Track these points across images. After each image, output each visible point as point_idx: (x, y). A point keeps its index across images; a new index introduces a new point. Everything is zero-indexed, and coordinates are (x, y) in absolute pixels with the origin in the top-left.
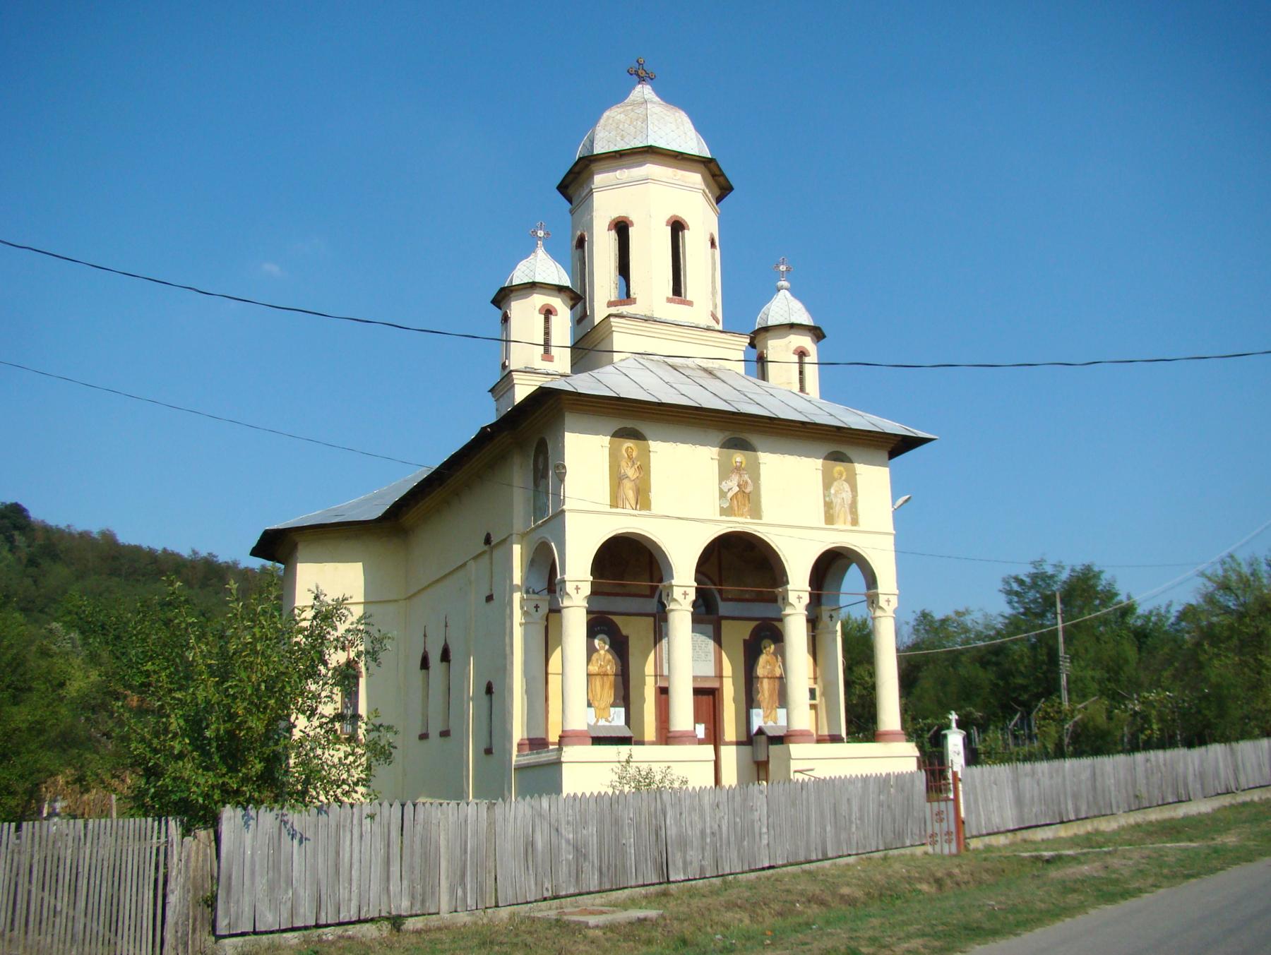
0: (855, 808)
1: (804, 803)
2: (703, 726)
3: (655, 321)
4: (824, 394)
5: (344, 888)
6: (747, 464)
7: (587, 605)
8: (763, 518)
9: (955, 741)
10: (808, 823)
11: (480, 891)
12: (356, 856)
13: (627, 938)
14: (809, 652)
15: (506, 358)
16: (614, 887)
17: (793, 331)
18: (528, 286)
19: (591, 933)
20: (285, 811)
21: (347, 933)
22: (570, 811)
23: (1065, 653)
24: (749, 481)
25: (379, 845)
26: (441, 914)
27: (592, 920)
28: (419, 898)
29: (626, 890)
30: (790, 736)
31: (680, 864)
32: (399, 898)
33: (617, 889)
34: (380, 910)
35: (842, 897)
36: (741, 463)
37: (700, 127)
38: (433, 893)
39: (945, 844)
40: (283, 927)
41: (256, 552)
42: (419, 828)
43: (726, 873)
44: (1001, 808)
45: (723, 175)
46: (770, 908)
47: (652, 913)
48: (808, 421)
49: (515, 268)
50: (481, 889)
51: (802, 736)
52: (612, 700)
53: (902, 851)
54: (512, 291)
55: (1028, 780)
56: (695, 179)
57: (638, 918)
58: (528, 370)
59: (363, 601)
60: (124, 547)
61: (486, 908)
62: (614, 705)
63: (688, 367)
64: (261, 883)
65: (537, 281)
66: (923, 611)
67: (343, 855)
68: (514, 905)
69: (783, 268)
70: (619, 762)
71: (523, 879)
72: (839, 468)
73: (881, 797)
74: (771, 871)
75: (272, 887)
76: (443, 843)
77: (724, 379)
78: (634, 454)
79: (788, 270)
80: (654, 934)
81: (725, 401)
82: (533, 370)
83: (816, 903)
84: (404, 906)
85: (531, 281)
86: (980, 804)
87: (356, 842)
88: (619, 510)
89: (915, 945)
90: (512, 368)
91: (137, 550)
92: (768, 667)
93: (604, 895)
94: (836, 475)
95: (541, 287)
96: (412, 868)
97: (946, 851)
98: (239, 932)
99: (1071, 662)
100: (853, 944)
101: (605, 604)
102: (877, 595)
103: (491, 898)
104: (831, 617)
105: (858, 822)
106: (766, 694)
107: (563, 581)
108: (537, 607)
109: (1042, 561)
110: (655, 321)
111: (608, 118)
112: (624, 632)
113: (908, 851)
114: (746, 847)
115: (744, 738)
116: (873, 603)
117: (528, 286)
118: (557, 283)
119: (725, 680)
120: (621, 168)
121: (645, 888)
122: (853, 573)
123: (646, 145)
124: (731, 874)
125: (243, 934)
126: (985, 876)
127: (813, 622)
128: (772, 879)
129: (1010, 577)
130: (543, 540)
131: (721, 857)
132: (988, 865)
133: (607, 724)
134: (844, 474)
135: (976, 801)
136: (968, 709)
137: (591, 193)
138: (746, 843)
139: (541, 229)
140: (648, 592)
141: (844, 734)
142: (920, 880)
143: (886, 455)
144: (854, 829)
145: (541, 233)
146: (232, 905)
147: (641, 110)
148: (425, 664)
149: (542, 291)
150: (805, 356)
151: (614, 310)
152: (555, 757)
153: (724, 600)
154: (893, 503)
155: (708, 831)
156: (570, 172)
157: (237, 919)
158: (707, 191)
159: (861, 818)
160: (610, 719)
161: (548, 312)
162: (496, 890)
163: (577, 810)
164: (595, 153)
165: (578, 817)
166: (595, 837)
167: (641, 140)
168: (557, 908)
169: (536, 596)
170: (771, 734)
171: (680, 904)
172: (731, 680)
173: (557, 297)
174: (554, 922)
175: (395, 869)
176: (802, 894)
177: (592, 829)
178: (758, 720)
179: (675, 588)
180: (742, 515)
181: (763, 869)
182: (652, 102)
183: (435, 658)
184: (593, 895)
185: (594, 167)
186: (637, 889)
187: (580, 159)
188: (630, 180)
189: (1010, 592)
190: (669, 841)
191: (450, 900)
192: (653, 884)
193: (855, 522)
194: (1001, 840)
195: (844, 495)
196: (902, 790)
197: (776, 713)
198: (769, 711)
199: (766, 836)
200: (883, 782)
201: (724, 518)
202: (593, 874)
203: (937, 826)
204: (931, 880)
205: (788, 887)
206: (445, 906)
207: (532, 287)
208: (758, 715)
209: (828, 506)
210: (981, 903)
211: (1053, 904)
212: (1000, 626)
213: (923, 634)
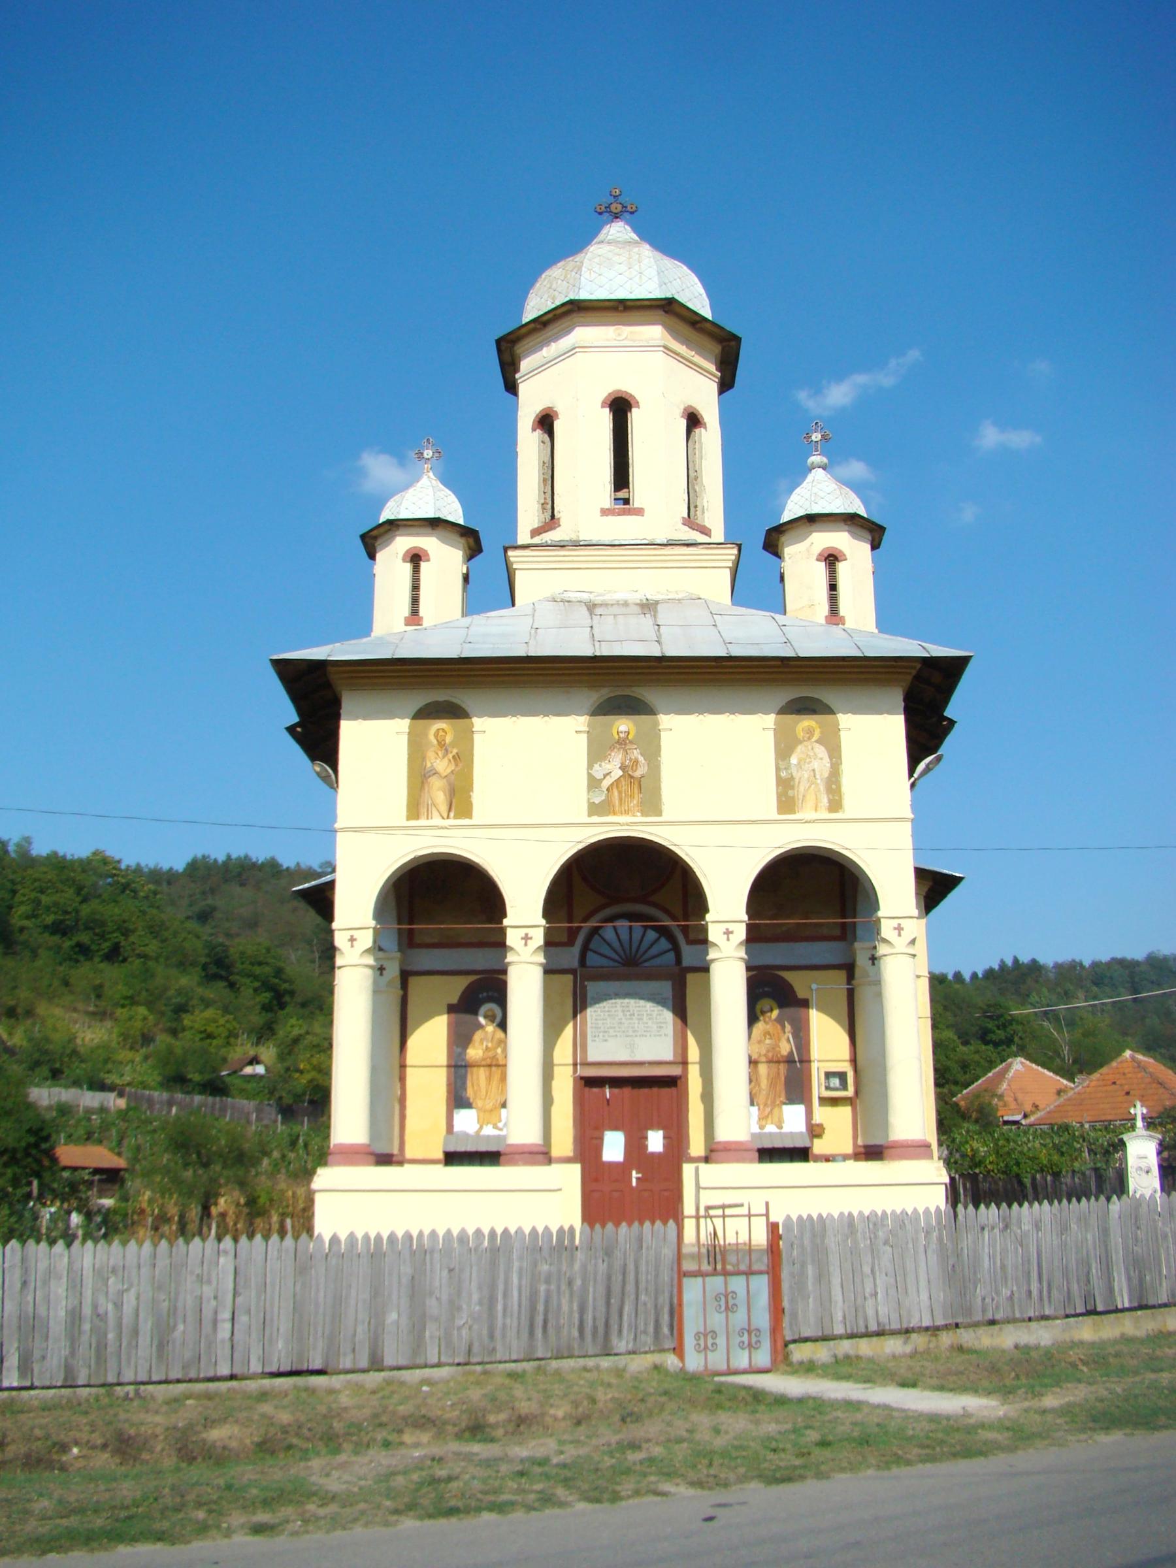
2: (661, 1133)
7: (746, 957)
8: (664, 814)
17: (817, 526)
24: (641, 759)
78: (448, 739)
79: (825, 438)
88: (422, 822)
92: (768, 1041)
95: (405, 526)
101: (775, 954)
119: (690, 1067)
120: (547, 342)
150: (838, 561)
160: (500, 1125)
161: (831, 559)
180: (627, 812)
185: (519, 348)
193: (835, 805)
195: (816, 765)
197: (781, 1112)
198: (768, 1110)
201: (595, 819)
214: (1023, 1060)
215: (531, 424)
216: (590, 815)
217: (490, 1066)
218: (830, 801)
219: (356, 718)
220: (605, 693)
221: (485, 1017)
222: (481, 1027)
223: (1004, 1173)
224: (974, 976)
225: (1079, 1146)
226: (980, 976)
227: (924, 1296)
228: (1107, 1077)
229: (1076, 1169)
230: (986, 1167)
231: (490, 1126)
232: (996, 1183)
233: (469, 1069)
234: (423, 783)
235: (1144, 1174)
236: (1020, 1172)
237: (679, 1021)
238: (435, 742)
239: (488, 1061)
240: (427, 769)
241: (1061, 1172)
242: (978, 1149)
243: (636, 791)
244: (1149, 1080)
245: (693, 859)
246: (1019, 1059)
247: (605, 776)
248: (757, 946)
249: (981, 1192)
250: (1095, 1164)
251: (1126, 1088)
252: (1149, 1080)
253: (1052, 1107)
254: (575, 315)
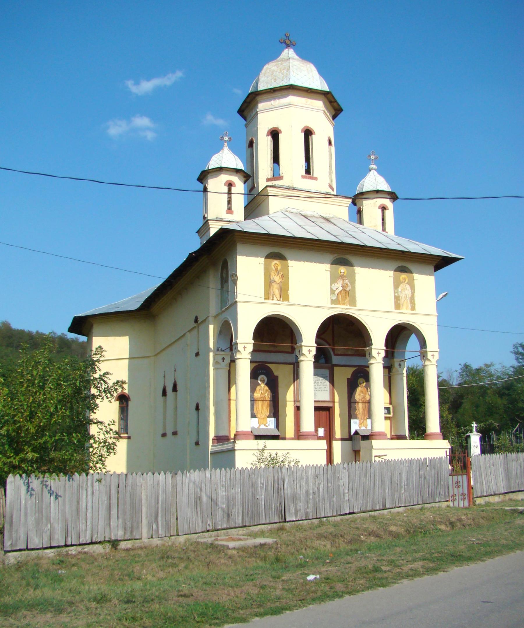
0: (404, 479)
1: (372, 475)
2: (323, 429)
3: (295, 189)
4: (397, 232)
5: (82, 524)
6: (347, 273)
7: (251, 358)
8: (357, 306)
9: (475, 439)
10: (374, 488)
11: (168, 527)
12: (90, 505)
13: (252, 555)
14: (385, 387)
15: (206, 213)
16: (251, 524)
18: (218, 169)
19: (230, 552)
20: (46, 479)
21: (84, 550)
22: (224, 479)
24: (349, 283)
25: (104, 498)
26: (143, 539)
27: (231, 544)
28: (129, 529)
29: (259, 526)
30: (373, 435)
31: (293, 511)
32: (116, 530)
33: (255, 525)
34: (105, 537)
35: (390, 532)
36: (344, 273)
37: (322, 72)
38: (138, 527)
39: (460, 500)
40: (45, 546)
41: (71, 330)
42: (129, 488)
43: (322, 516)
44: (496, 480)
45: (336, 102)
46: (344, 538)
47: (269, 540)
48: (384, 247)
49: (210, 160)
50: (168, 525)
51: (381, 435)
52: (268, 413)
53: (433, 505)
54: (209, 173)
55: (513, 463)
56: (319, 104)
57: (261, 543)
58: (218, 219)
59: (128, 357)
60: (15, 330)
61: (171, 536)
62: (269, 417)
63: (314, 217)
64: (31, 520)
65: (223, 166)
66: (465, 364)
67: (82, 504)
68: (188, 534)
69: (373, 157)
70: (258, 450)
71: (194, 518)
72: (403, 276)
73: (421, 472)
74: (351, 516)
75: (38, 522)
76: (143, 497)
77: (335, 223)
80: (269, 553)
81: (334, 236)
82: (221, 219)
83: (373, 536)
84: (120, 534)
85: (219, 166)
86: (483, 478)
87: (89, 497)
88: (270, 301)
89: (417, 566)
90: (209, 218)
91: (22, 332)
92: (362, 395)
93: (245, 529)
94: (402, 280)
95: (226, 170)
96: (125, 513)
97: (461, 505)
98: (18, 549)
100: (379, 564)
101: (262, 357)
102: (427, 352)
103: (174, 530)
104: (400, 365)
105: (406, 487)
106: (361, 410)
107: (237, 344)
108: (223, 359)
110: (295, 189)
111: (267, 69)
112: (276, 374)
113: (437, 505)
114: (335, 501)
115: (347, 436)
116: (424, 357)
117: (218, 169)
118: (235, 167)
119: (336, 403)
120: (274, 99)
121: (270, 525)
122: (413, 339)
123: (289, 84)
124: (325, 517)
125: (20, 550)
126: (482, 521)
127: (388, 368)
128: (350, 520)
129: (517, 344)
130: (226, 319)
131: (319, 507)
132: (484, 514)
133: (265, 427)
134: (407, 279)
135: (481, 476)
136: (490, 421)
137: (256, 114)
138: (334, 499)
139: (226, 136)
140: (290, 351)
141: (407, 434)
142: (440, 523)
143: (432, 268)
144: (403, 491)
145: (226, 138)
146: (13, 533)
147: (286, 64)
148: (164, 393)
149: (227, 172)
151: (270, 183)
152: (232, 447)
153: (335, 355)
154: (437, 297)
155: (311, 491)
156: (245, 102)
157: (16, 541)
158: (326, 112)
159: (408, 485)
160: (267, 425)
162: (177, 525)
163: (228, 479)
164: (259, 90)
165: (229, 482)
166: (240, 494)
167: (286, 82)
168: (215, 536)
169: (223, 353)
170: (362, 434)
171: (289, 535)
172: (338, 403)
173: (235, 176)
174: (209, 545)
175: (114, 512)
176: (365, 530)
177: (238, 489)
178: (355, 426)
179: (303, 347)
180: (344, 304)
181: (346, 514)
182: (293, 59)
183: (169, 389)
184: (238, 529)
185: (259, 98)
186: (266, 526)
187: (250, 94)
188: (279, 105)
189: (517, 353)
190: (286, 497)
191: (148, 531)
192: (276, 523)
193: (413, 308)
194: (496, 499)
195: (407, 292)
196: (434, 468)
198: (362, 421)
199: (347, 495)
200: (422, 463)
201: (333, 306)
202: (238, 516)
203: (456, 490)
204: (448, 523)
205: (357, 526)
206: (145, 533)
207: (220, 170)
208: (355, 423)
209: (397, 299)
210: (466, 539)
211: (512, 541)
212: (510, 373)
213: (466, 378)
215: (266, 132)
216: (331, 304)
217: (263, 401)
218: (411, 306)
219: (243, 255)
220: (336, 256)
221: (261, 381)
222: (259, 384)
227: (502, 483)
231: (263, 425)
233: (255, 402)
234: (270, 285)
235: (476, 448)
237: (331, 386)
238: (274, 269)
239: (262, 399)
240: (271, 280)
243: (347, 296)
245: (367, 324)
247: (336, 289)
248: (256, 354)
254: (290, 90)
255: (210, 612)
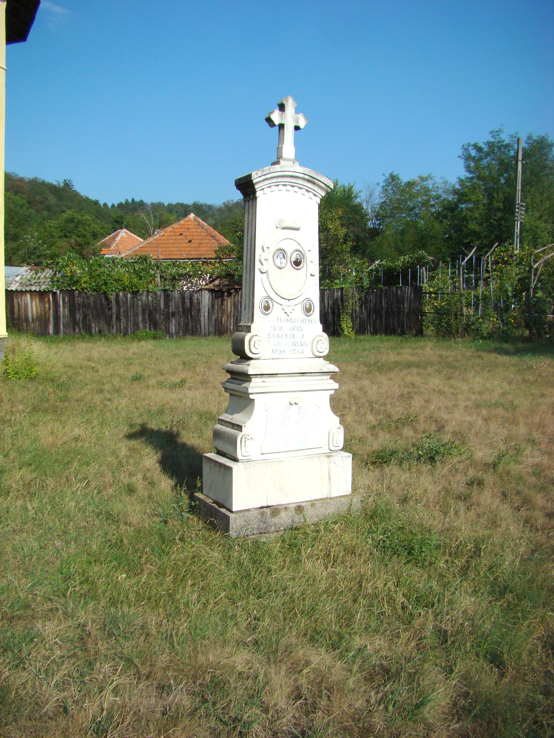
23: (522, 201)
66: (391, 173)
99: (526, 211)
109: (499, 131)
129: (469, 145)
189: (468, 158)
214: (126, 231)
223: (94, 290)
224: (113, 206)
225: (153, 272)
226: (116, 206)
228: (177, 230)
229: (150, 290)
230: (81, 285)
232: (88, 298)
236: (107, 290)
241: (138, 291)
242: (75, 271)
244: (205, 234)
246: (124, 230)
249: (77, 305)
250: (164, 287)
251: (189, 238)
252: (205, 234)
253: (138, 248)
255: (485, 500)
